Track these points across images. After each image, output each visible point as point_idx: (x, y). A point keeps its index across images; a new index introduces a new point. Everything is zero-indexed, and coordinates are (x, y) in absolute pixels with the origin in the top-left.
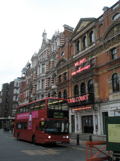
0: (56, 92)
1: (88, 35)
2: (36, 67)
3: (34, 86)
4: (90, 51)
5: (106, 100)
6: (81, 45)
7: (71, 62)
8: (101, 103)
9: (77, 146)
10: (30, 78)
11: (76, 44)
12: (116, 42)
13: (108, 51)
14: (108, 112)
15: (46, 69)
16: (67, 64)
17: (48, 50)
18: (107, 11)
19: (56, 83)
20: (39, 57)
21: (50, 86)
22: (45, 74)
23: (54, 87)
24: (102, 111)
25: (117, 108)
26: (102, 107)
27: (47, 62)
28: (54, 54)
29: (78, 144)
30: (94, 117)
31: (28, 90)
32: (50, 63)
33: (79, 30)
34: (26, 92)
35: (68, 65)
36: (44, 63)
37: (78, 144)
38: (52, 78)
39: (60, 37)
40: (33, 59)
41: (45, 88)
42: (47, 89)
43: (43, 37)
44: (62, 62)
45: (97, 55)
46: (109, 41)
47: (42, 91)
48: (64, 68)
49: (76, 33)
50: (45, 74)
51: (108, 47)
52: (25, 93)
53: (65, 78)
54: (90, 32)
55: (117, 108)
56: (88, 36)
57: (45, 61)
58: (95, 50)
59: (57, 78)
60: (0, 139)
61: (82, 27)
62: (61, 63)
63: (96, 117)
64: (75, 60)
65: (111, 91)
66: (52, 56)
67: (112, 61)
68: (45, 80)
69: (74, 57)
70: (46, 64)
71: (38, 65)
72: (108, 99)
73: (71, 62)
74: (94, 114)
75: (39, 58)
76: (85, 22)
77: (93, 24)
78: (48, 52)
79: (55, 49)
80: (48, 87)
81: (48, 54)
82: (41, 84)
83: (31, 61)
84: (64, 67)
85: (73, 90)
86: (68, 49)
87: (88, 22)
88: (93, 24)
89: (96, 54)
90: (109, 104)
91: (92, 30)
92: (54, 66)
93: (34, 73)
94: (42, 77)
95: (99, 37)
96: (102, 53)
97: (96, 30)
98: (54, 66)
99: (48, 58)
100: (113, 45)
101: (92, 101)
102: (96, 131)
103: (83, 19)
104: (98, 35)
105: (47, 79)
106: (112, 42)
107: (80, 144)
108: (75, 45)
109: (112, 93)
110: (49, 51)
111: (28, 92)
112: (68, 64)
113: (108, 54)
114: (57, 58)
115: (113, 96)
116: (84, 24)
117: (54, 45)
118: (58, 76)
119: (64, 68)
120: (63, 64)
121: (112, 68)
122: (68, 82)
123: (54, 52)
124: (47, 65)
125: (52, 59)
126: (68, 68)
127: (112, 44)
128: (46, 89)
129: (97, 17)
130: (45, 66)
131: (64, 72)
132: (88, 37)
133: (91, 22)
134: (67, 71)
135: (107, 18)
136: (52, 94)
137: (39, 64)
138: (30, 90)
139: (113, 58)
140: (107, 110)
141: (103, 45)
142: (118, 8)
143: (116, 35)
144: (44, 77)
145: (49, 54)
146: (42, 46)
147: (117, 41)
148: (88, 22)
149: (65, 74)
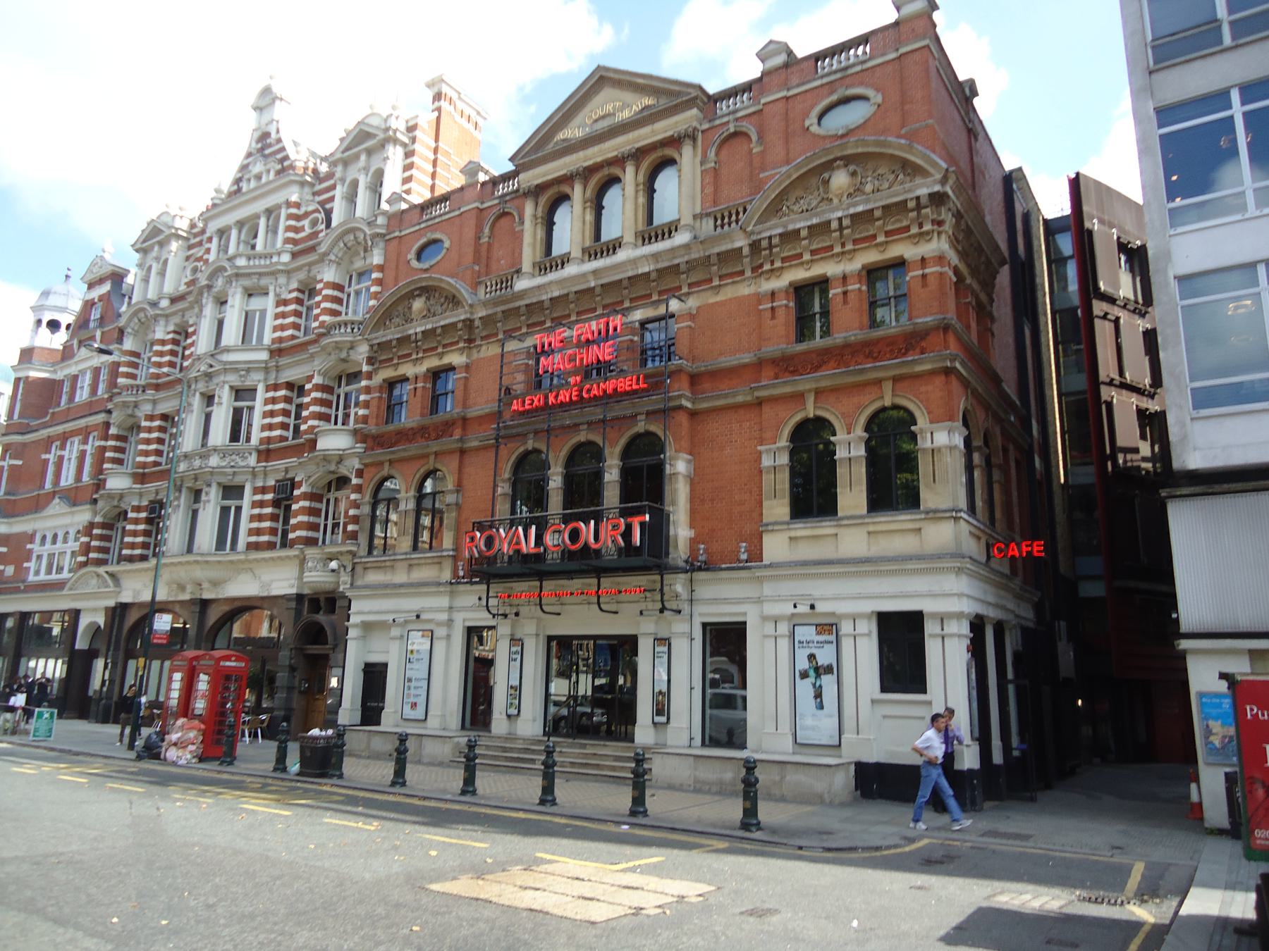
0: (126, 512)
1: (695, 155)
2: (174, 300)
3: (151, 418)
4: (646, 269)
5: (744, 557)
6: (584, 222)
7: (499, 309)
8: (707, 570)
9: (463, 798)
10: (118, 364)
11: (540, 209)
12: (414, 357)
13: (780, 290)
14: (745, 623)
15: (270, 323)
16: (462, 317)
17: (298, 205)
18: (786, 65)
19: (356, 422)
20: (215, 240)
21: (163, 460)
22: (264, 356)
23: (334, 441)
24: (700, 615)
25: (812, 607)
26: (703, 592)
27: (282, 280)
28: (141, 315)
29: (550, 798)
30: (645, 647)
31: (85, 442)
32: (308, 290)
33: (573, 132)
34: (63, 447)
35: (469, 324)
36: (264, 282)
37: (550, 798)
38: (318, 388)
39: (312, 185)
40: (154, 238)
41: (254, 441)
42: (268, 451)
43: (254, 114)
44: (423, 299)
45: (723, 290)
46: (790, 237)
47: (228, 460)
48: (434, 339)
49: (550, 147)
50: (264, 356)
51: (850, 252)
52: (51, 457)
53: (435, 401)
54: (658, 160)
55: (812, 607)
56: (540, 213)
57: (273, 274)
58: (688, 271)
59: (368, 390)
60: (42, 799)
61: (603, 117)
62: (418, 304)
63: (666, 649)
64: (528, 302)
65: (777, 508)
66: (336, 250)
67: (428, 421)
68: (261, 394)
69: (521, 284)
70: (277, 295)
71: (209, 287)
72: (756, 555)
73: (499, 309)
74: (645, 630)
75: (214, 246)
76: (628, 96)
77: (688, 119)
78: (298, 218)
79: (151, 295)
80: (156, 464)
81: (297, 230)
82: (228, 411)
83: (137, 256)
84: (439, 331)
85: (503, 481)
86: (479, 228)
87: (647, 101)
88: (688, 119)
89: (688, 294)
90: (760, 580)
91: (566, 189)
92: (339, 313)
93: (160, 334)
94: (237, 370)
95: (715, 203)
96: (729, 293)
97: (699, 158)
98: (339, 313)
99: (295, 255)
100: (782, 268)
101: (649, 556)
102: (509, 716)
103: (611, 75)
104: (710, 190)
105: (276, 387)
106: (528, 319)
107: (480, 791)
108: (535, 216)
109: (788, 523)
110: (307, 214)
111: (83, 453)
112: (472, 321)
113: (773, 308)
114: (381, 268)
115: (791, 538)
116: (618, 106)
117: (150, 267)
118: (378, 379)
119: (434, 339)
120: (429, 314)
121: (881, 375)
122: (460, 423)
123: (143, 310)
124: (285, 303)
125: (334, 267)
126: (470, 341)
127: (807, 257)
128: (259, 452)
129: (712, 88)
130: (268, 304)
131: (434, 362)
132: (637, 185)
133: (664, 102)
134: (456, 359)
135: (781, 105)
136: (104, 516)
137: (220, 282)
138: (106, 437)
139: (434, 408)
140: (745, 614)
141: (746, 251)
142: (858, 68)
143: (840, 214)
144: (248, 370)
145: (308, 231)
146: (244, 168)
147: (843, 245)
148: (647, 101)
149: (436, 375)
